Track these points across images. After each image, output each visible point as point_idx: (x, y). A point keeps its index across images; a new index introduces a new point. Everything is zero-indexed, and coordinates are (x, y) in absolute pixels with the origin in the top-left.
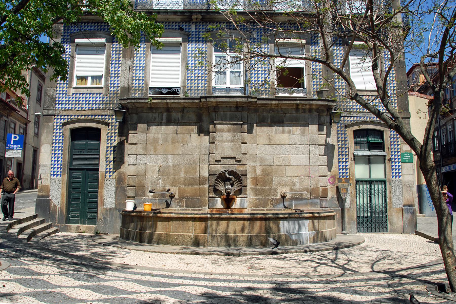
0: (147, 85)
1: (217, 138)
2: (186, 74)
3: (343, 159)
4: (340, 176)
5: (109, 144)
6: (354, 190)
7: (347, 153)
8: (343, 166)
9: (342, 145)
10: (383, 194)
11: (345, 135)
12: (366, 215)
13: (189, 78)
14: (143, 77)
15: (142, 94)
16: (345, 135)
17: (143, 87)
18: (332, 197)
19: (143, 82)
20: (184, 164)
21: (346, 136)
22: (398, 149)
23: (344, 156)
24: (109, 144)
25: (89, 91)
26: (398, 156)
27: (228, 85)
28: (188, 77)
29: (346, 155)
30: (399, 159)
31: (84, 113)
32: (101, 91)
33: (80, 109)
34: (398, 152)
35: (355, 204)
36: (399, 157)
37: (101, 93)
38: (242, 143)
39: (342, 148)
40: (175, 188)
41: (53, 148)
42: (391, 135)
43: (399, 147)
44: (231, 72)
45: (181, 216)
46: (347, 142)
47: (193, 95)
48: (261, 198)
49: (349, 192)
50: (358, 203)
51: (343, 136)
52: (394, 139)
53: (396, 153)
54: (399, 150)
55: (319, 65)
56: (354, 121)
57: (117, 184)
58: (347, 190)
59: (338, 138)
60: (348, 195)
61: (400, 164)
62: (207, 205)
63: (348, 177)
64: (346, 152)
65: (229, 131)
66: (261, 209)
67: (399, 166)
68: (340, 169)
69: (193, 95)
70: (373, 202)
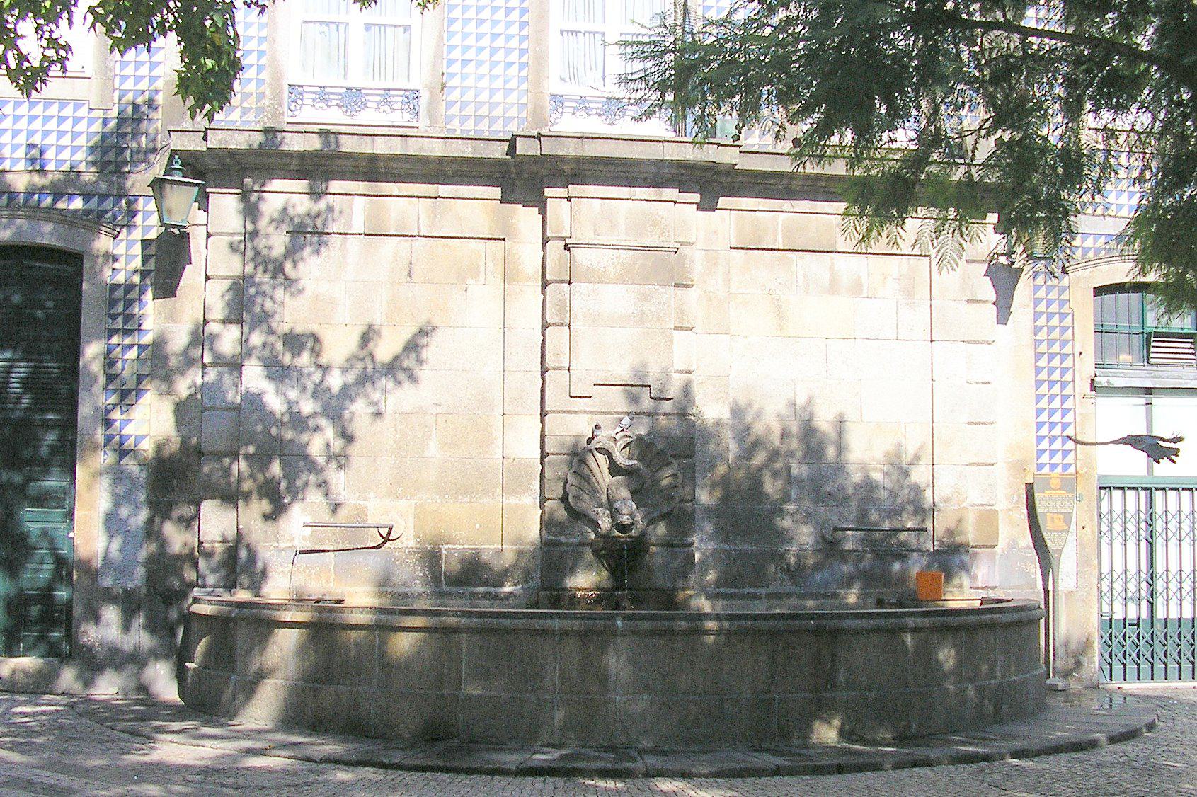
0: (277, 76)
1: (577, 304)
2: (440, 37)
4: (1040, 467)
5: (120, 319)
6: (1091, 519)
7: (1068, 377)
9: (1051, 343)
10: (1143, 534)
11: (1061, 305)
12: (1132, 615)
13: (456, 54)
14: (261, 40)
15: (260, 110)
16: (1061, 305)
17: (261, 82)
18: (1013, 545)
19: (263, 61)
20: (439, 410)
21: (1065, 309)
23: (1056, 389)
24: (120, 319)
27: (357, 79)
28: (451, 48)
29: (1064, 385)
35: (1096, 574)
37: (78, 104)
38: (676, 328)
39: (1051, 357)
40: (402, 504)
44: (368, 27)
45: (506, 622)
46: (1068, 335)
47: (470, 124)
48: (747, 547)
49: (1073, 527)
50: (1105, 570)
51: (1054, 308)
55: (724, 14)
57: (154, 490)
58: (1067, 518)
59: (1037, 316)
60: (1072, 537)
62: (792, 589)
63: (1072, 470)
64: (1064, 371)
65: (624, 278)
66: (747, 590)
68: (1040, 439)
69: (470, 124)
70: (1160, 567)
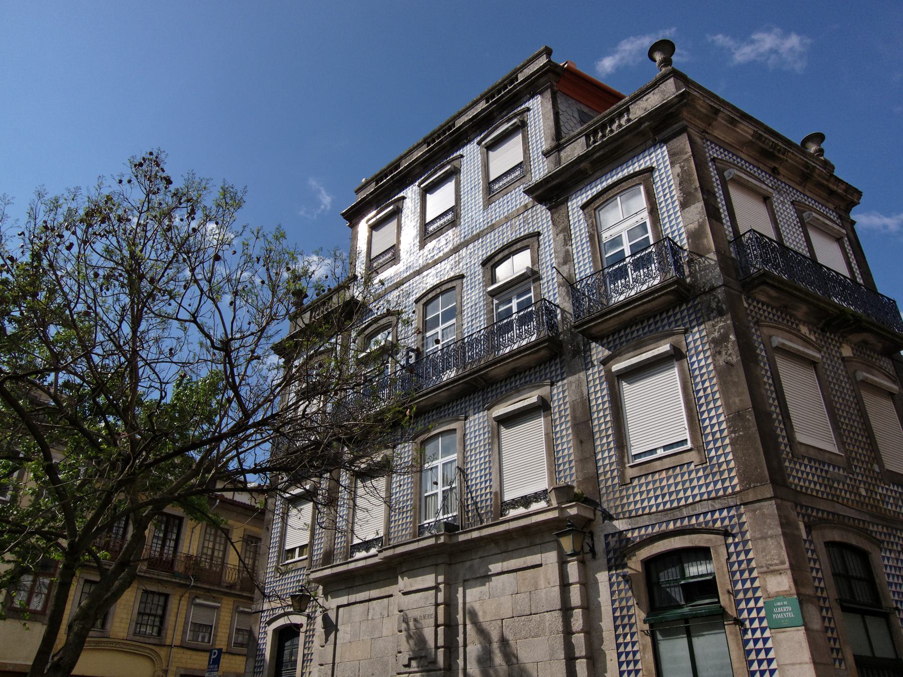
3: (625, 636)
8: (627, 654)
22: (755, 590)
25: (667, 463)
26: (759, 610)
30: (761, 620)
31: (699, 509)
32: (686, 458)
33: (690, 500)
34: (757, 600)
36: (763, 614)
37: (689, 464)
41: (618, 614)
42: (729, 555)
43: (756, 584)
52: (739, 566)
53: (752, 604)
54: (759, 594)
56: (641, 536)
61: (767, 634)
67: (765, 640)
